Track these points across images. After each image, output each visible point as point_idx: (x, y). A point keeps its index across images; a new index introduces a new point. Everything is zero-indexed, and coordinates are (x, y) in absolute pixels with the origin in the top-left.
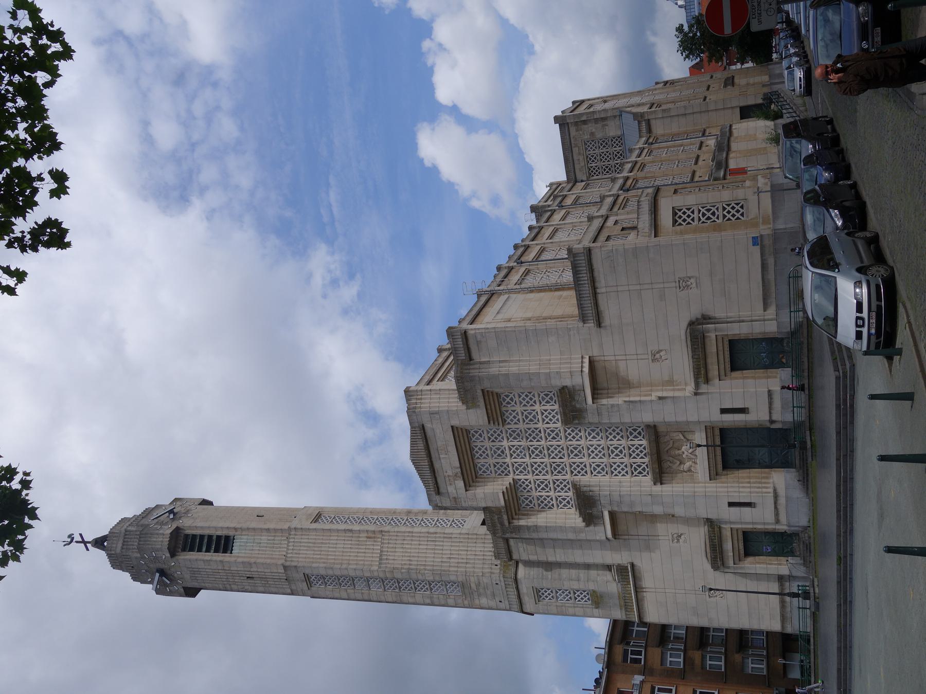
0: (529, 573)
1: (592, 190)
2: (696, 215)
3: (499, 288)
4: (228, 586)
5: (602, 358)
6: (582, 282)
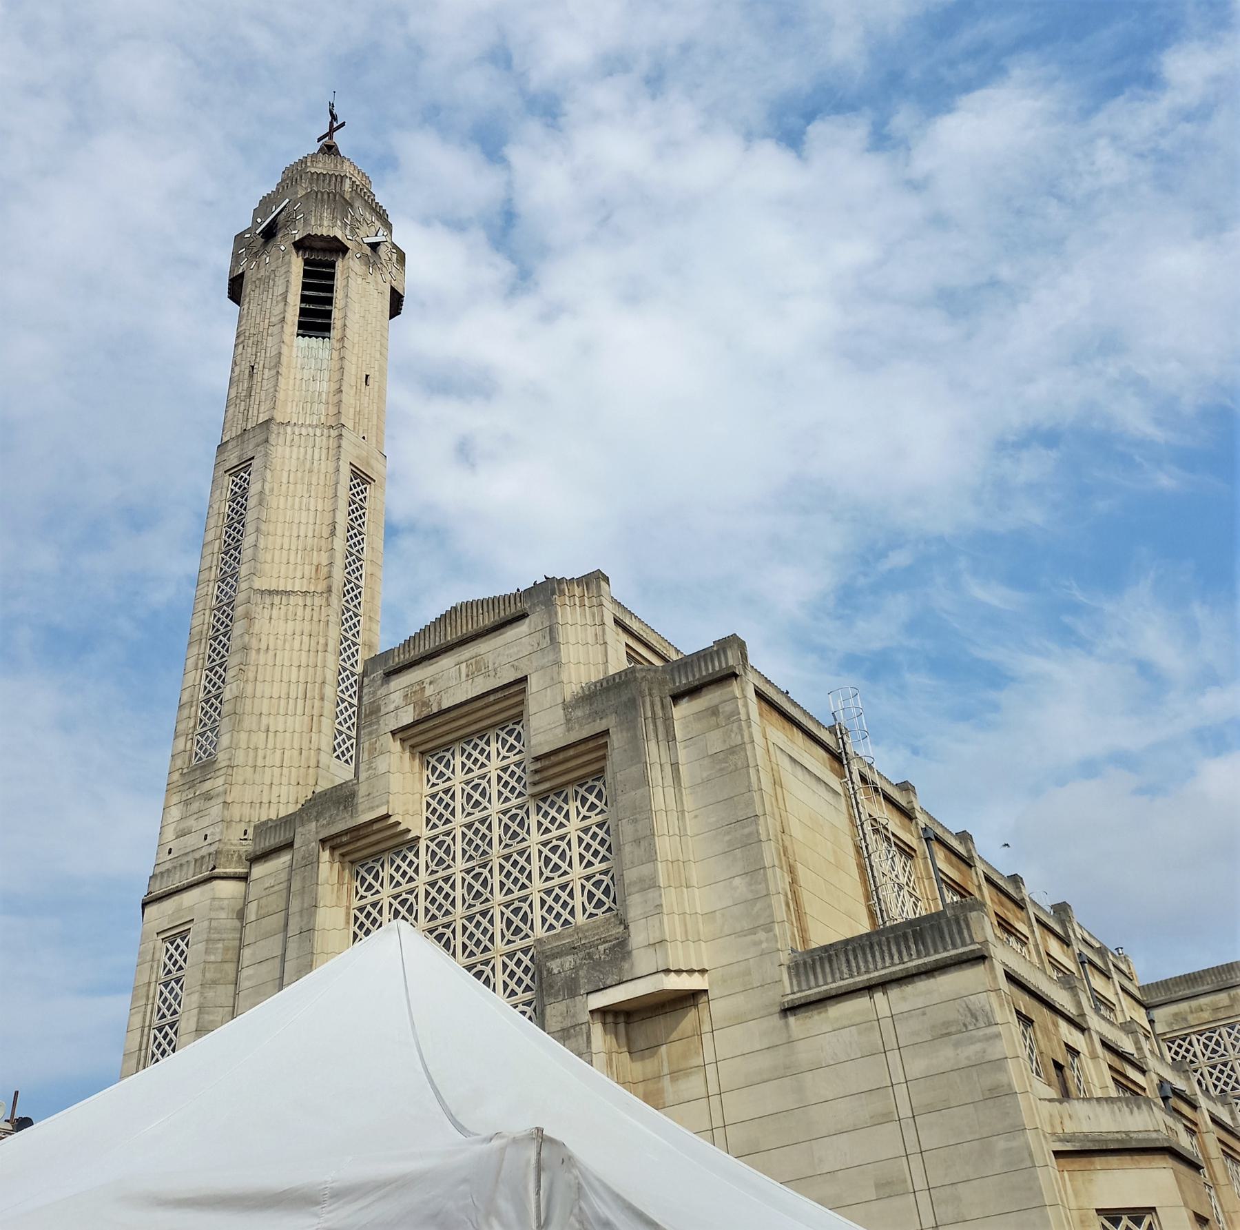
0: (223, 909)
3: (856, 777)
4: (242, 339)
5: (706, 1028)
6: (894, 950)
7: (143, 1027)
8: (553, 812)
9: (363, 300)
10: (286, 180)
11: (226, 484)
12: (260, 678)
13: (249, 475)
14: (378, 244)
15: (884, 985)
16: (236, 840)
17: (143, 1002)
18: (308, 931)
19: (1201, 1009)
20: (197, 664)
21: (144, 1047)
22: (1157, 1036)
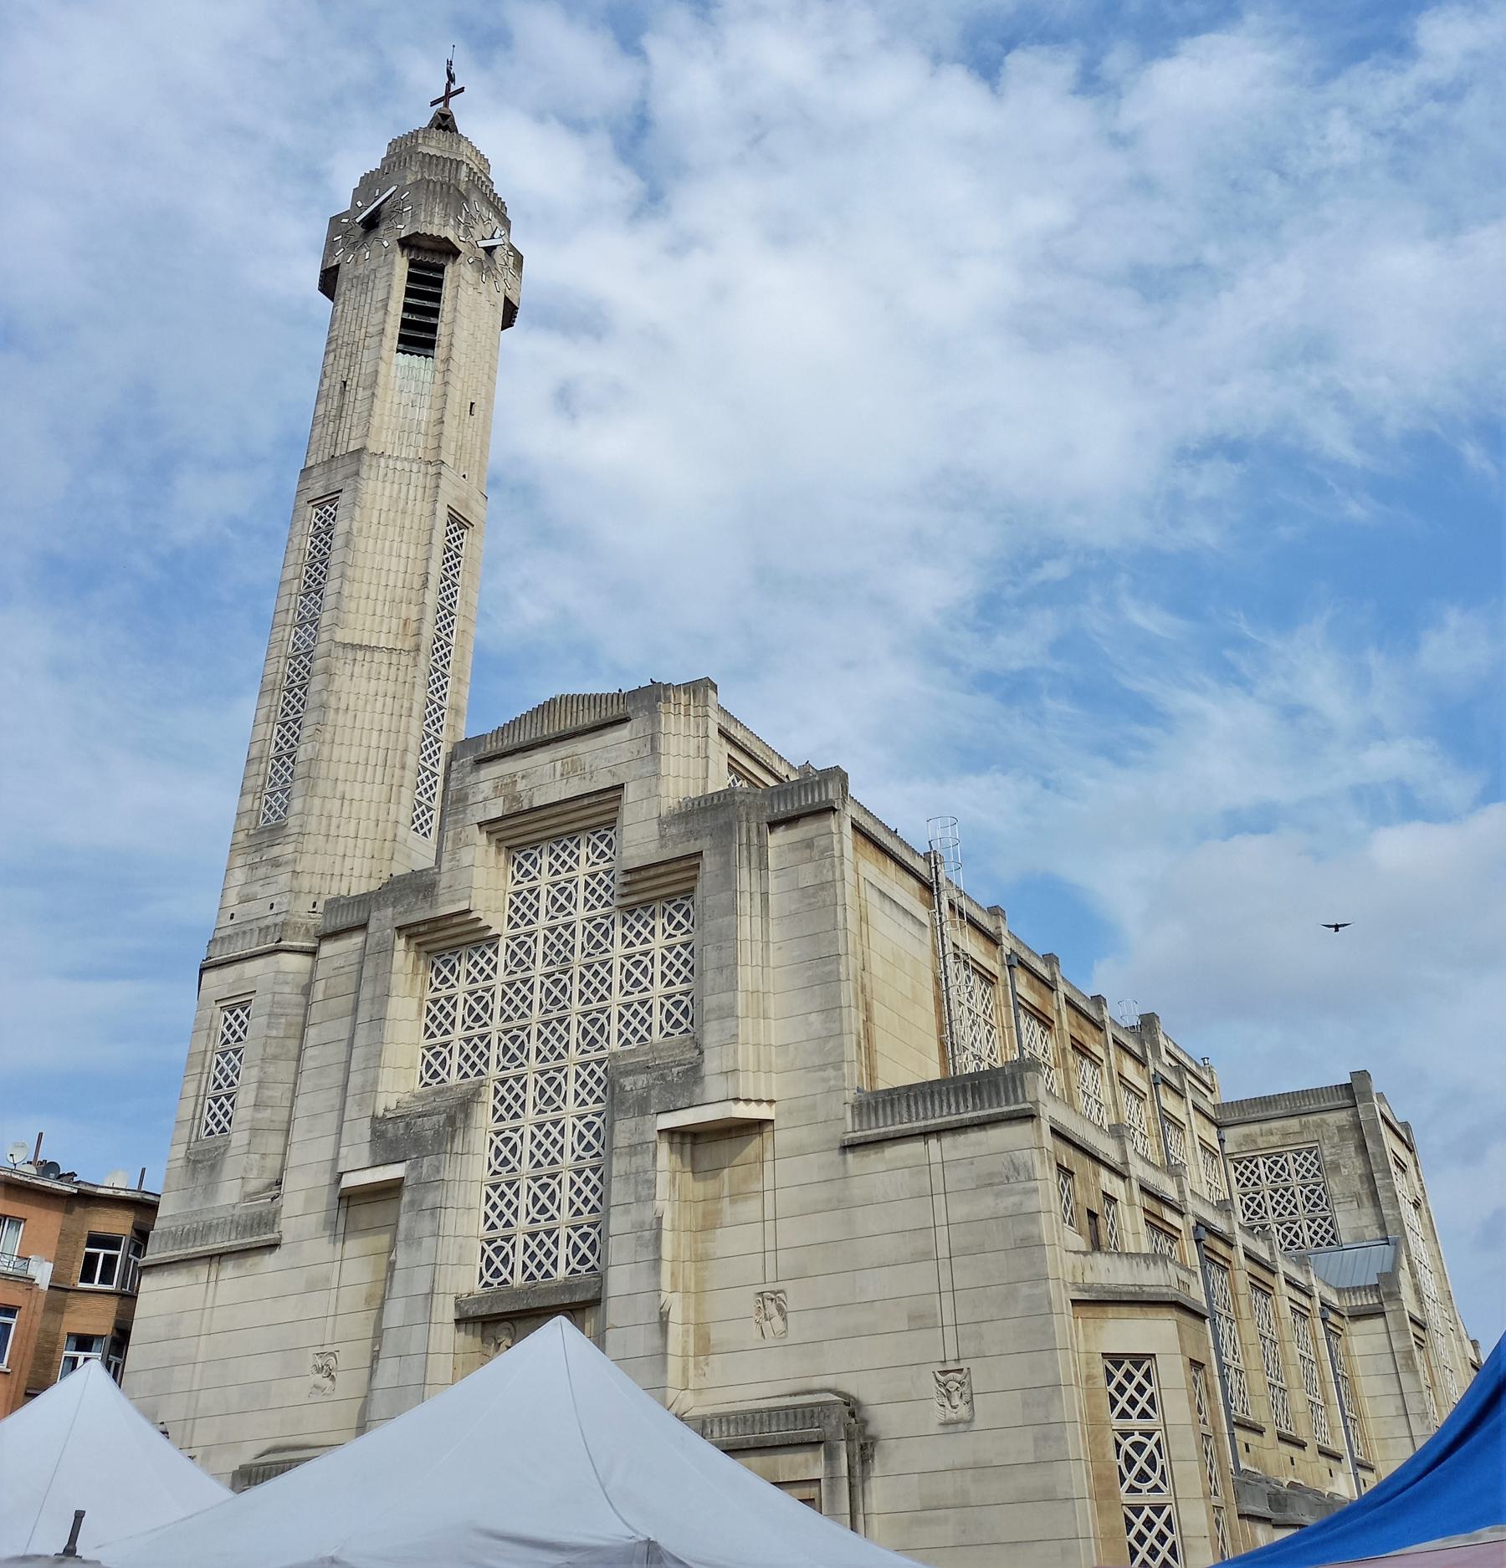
0: (287, 983)
1: (1201, 1163)
2: (1136, 1423)
4: (333, 346)
5: (768, 1156)
6: (952, 1100)
7: (198, 1096)
8: (638, 927)
9: (474, 313)
10: (392, 156)
11: (308, 516)
12: (338, 740)
13: (335, 509)
14: (494, 247)
15: (938, 1132)
16: (303, 911)
17: (199, 1070)
18: (379, 1020)
19: (1270, 1134)
20: (269, 717)
21: (197, 1116)
22: (1225, 1155)
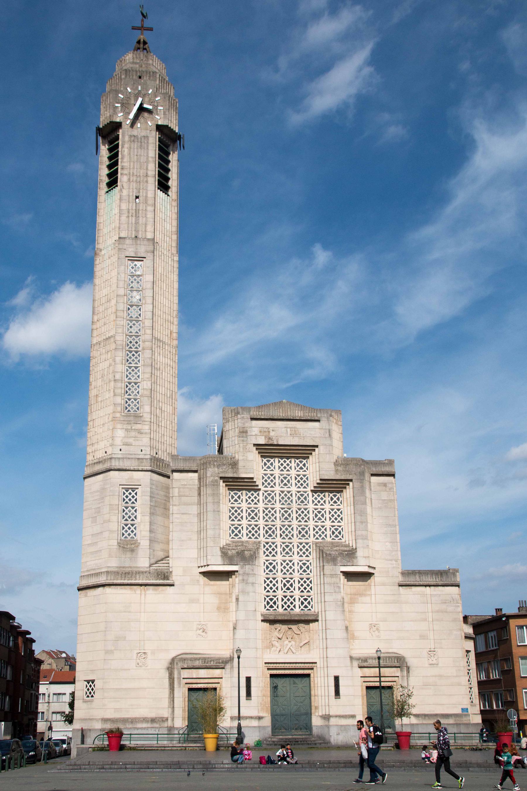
5: (373, 584)
